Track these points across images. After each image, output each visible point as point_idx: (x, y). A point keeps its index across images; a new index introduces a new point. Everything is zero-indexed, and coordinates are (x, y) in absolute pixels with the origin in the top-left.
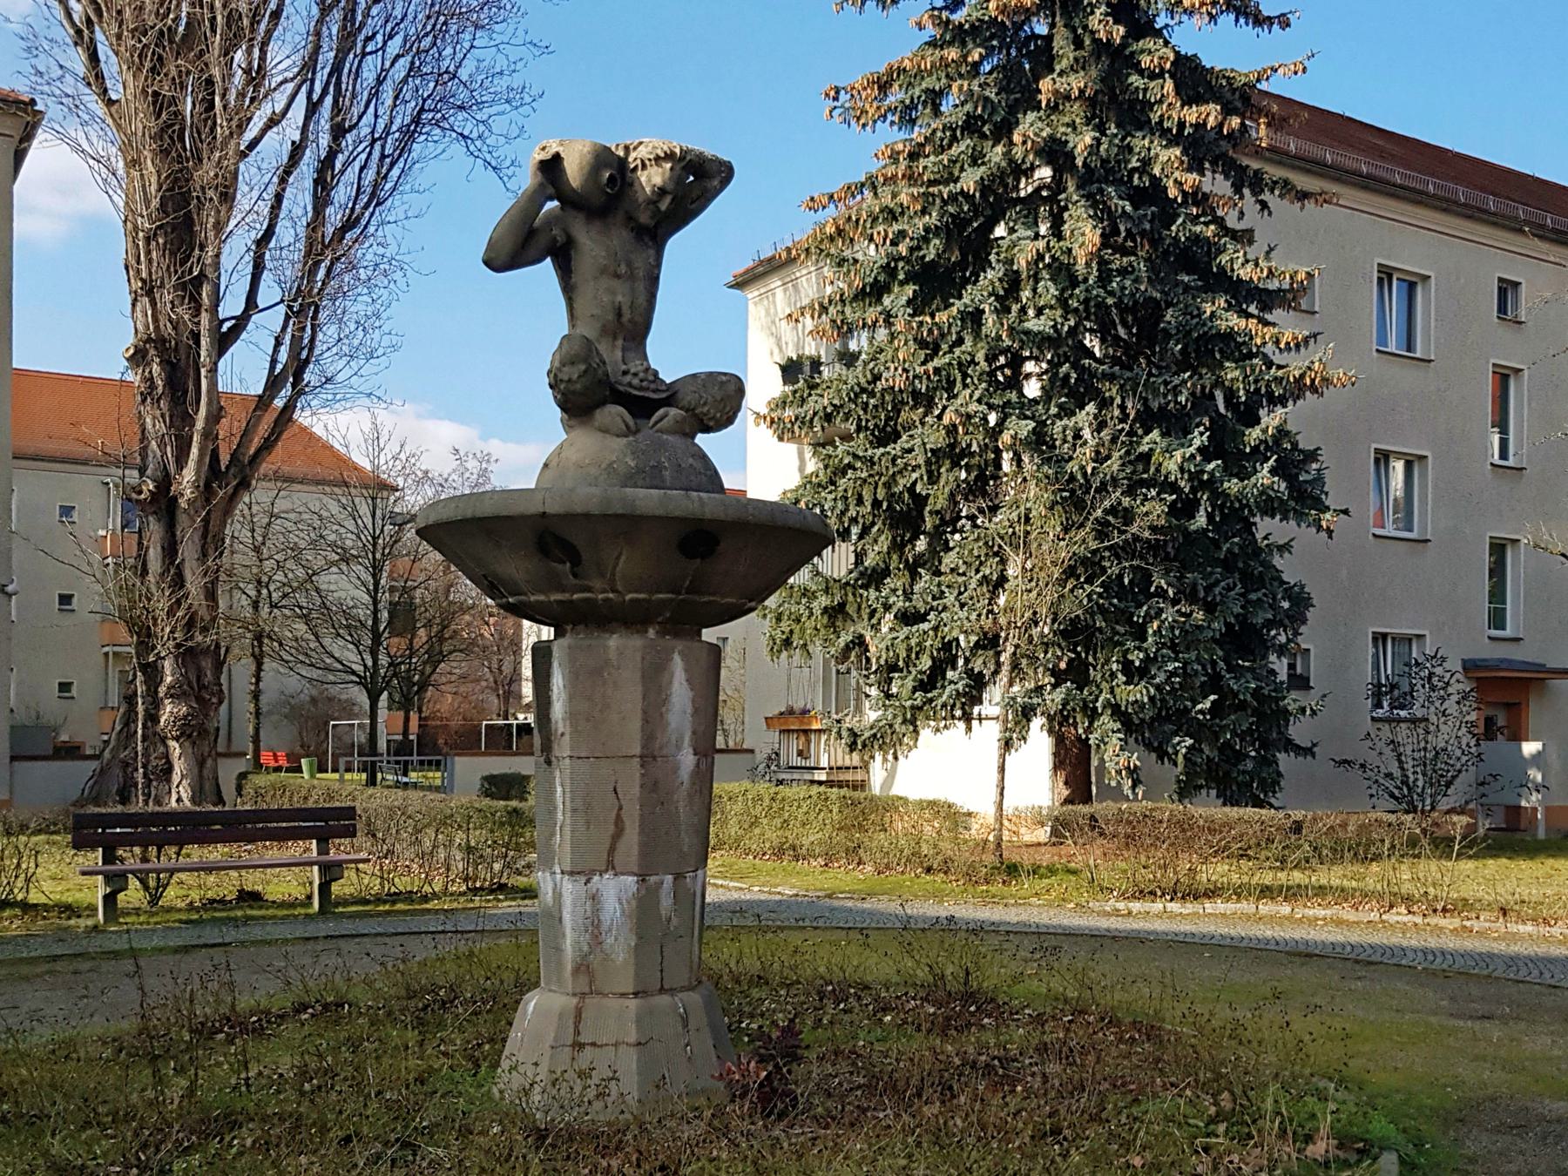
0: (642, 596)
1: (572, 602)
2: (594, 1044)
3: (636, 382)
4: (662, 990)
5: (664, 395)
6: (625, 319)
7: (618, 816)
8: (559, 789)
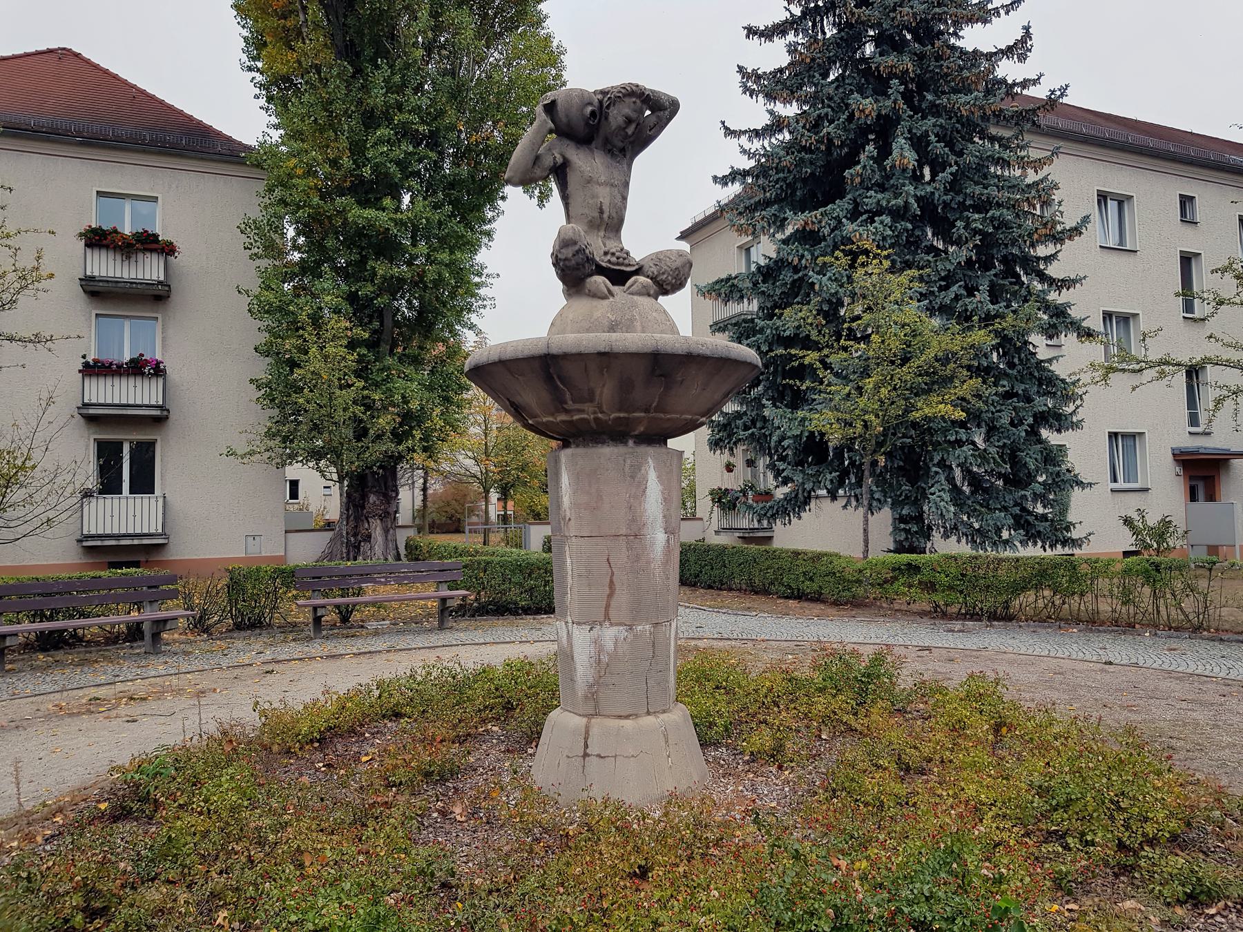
0: (622, 415)
1: (571, 422)
2: (599, 756)
3: (614, 259)
4: (648, 713)
5: (633, 269)
6: (605, 216)
7: (611, 582)
8: (569, 560)
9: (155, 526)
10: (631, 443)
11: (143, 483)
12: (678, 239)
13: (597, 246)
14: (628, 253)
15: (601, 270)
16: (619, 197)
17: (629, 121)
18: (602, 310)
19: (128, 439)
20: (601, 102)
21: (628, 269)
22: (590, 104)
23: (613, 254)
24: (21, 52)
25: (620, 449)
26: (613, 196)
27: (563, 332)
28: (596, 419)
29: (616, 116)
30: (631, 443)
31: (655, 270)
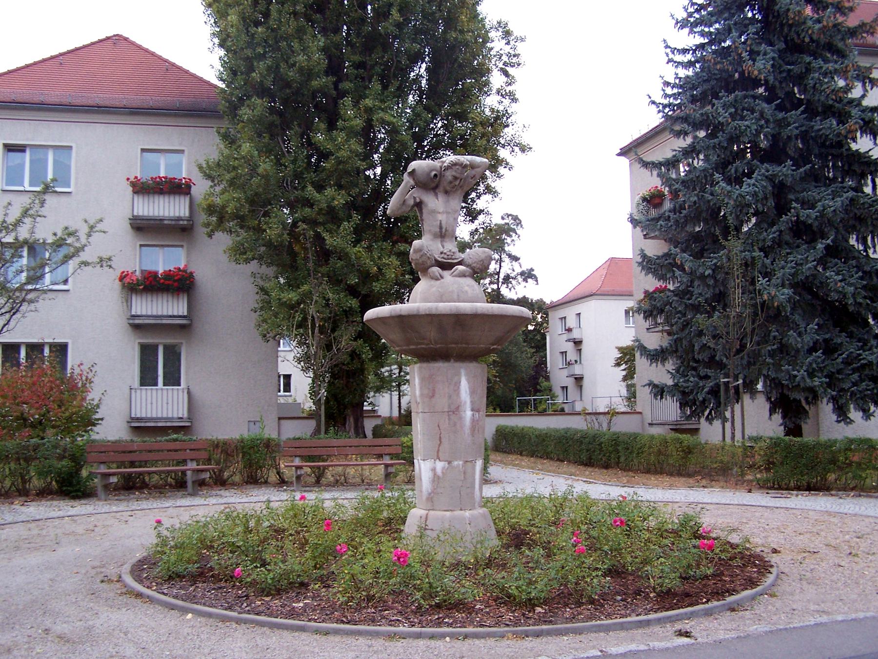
3: (446, 256)
9: (183, 412)
11: (173, 379)
12: (619, 155)
19: (161, 341)
24: (89, 42)
25: (446, 364)
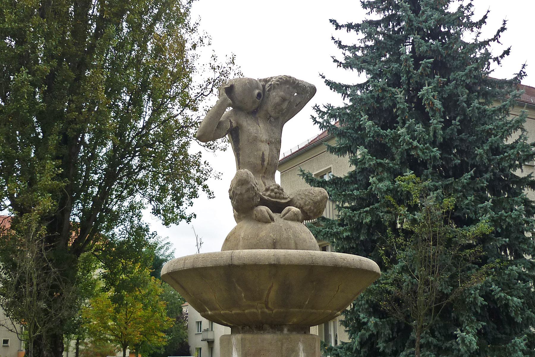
3: (273, 194)
6: (266, 163)
10: (286, 331)
13: (260, 185)
14: (282, 190)
15: (264, 202)
16: (275, 151)
17: (284, 100)
18: (266, 231)
20: (264, 86)
21: (283, 201)
22: (257, 88)
23: (272, 190)
26: (271, 150)
27: (236, 247)
28: (263, 313)
29: (275, 97)
30: (286, 331)
31: (301, 202)
